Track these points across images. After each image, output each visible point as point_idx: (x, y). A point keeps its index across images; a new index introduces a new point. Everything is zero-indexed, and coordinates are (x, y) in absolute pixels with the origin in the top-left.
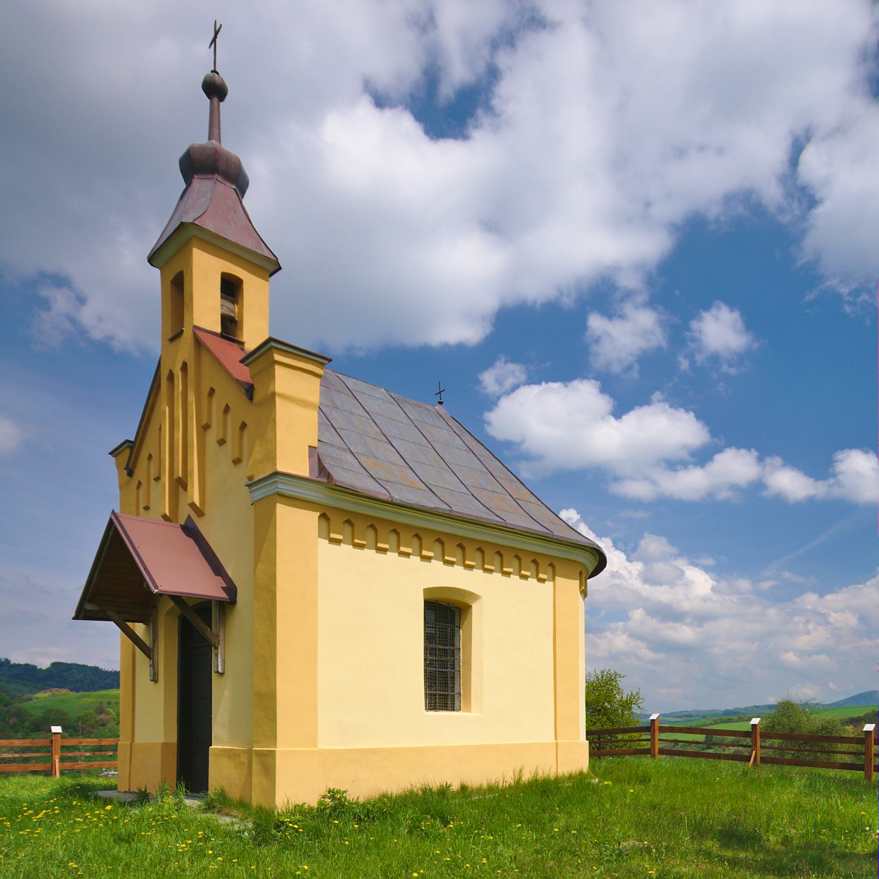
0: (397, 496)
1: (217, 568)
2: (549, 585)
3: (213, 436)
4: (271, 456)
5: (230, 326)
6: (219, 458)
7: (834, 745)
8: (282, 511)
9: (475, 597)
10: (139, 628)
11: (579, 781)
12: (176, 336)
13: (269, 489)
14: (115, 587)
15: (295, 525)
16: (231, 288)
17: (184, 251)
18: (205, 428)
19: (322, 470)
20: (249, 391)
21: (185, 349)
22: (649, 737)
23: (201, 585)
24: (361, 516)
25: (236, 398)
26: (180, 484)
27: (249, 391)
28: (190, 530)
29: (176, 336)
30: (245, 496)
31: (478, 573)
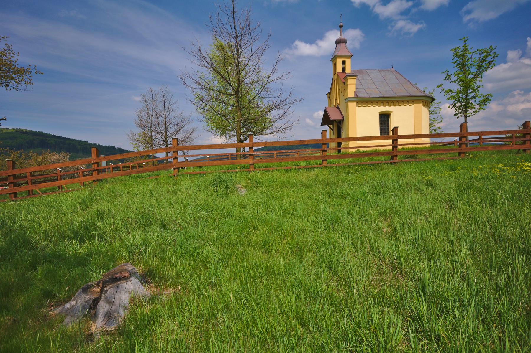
0: (371, 96)
1: (342, 114)
2: (413, 106)
3: (340, 91)
4: (348, 95)
5: (344, 69)
6: (341, 94)
7: (347, 143)
8: (349, 103)
9: (392, 112)
10: (331, 126)
11: (252, 141)
12: (335, 74)
13: (348, 100)
14: (326, 120)
15: (352, 105)
16: (344, 63)
17: (335, 59)
18: (339, 90)
19: (356, 95)
20: (344, 83)
21: (336, 76)
22: (400, 141)
23: (339, 117)
24: (363, 101)
25: (343, 84)
26: (336, 100)
27: (344, 83)
28: (338, 108)
29: (335, 74)
30: (344, 102)
31: (392, 107)
